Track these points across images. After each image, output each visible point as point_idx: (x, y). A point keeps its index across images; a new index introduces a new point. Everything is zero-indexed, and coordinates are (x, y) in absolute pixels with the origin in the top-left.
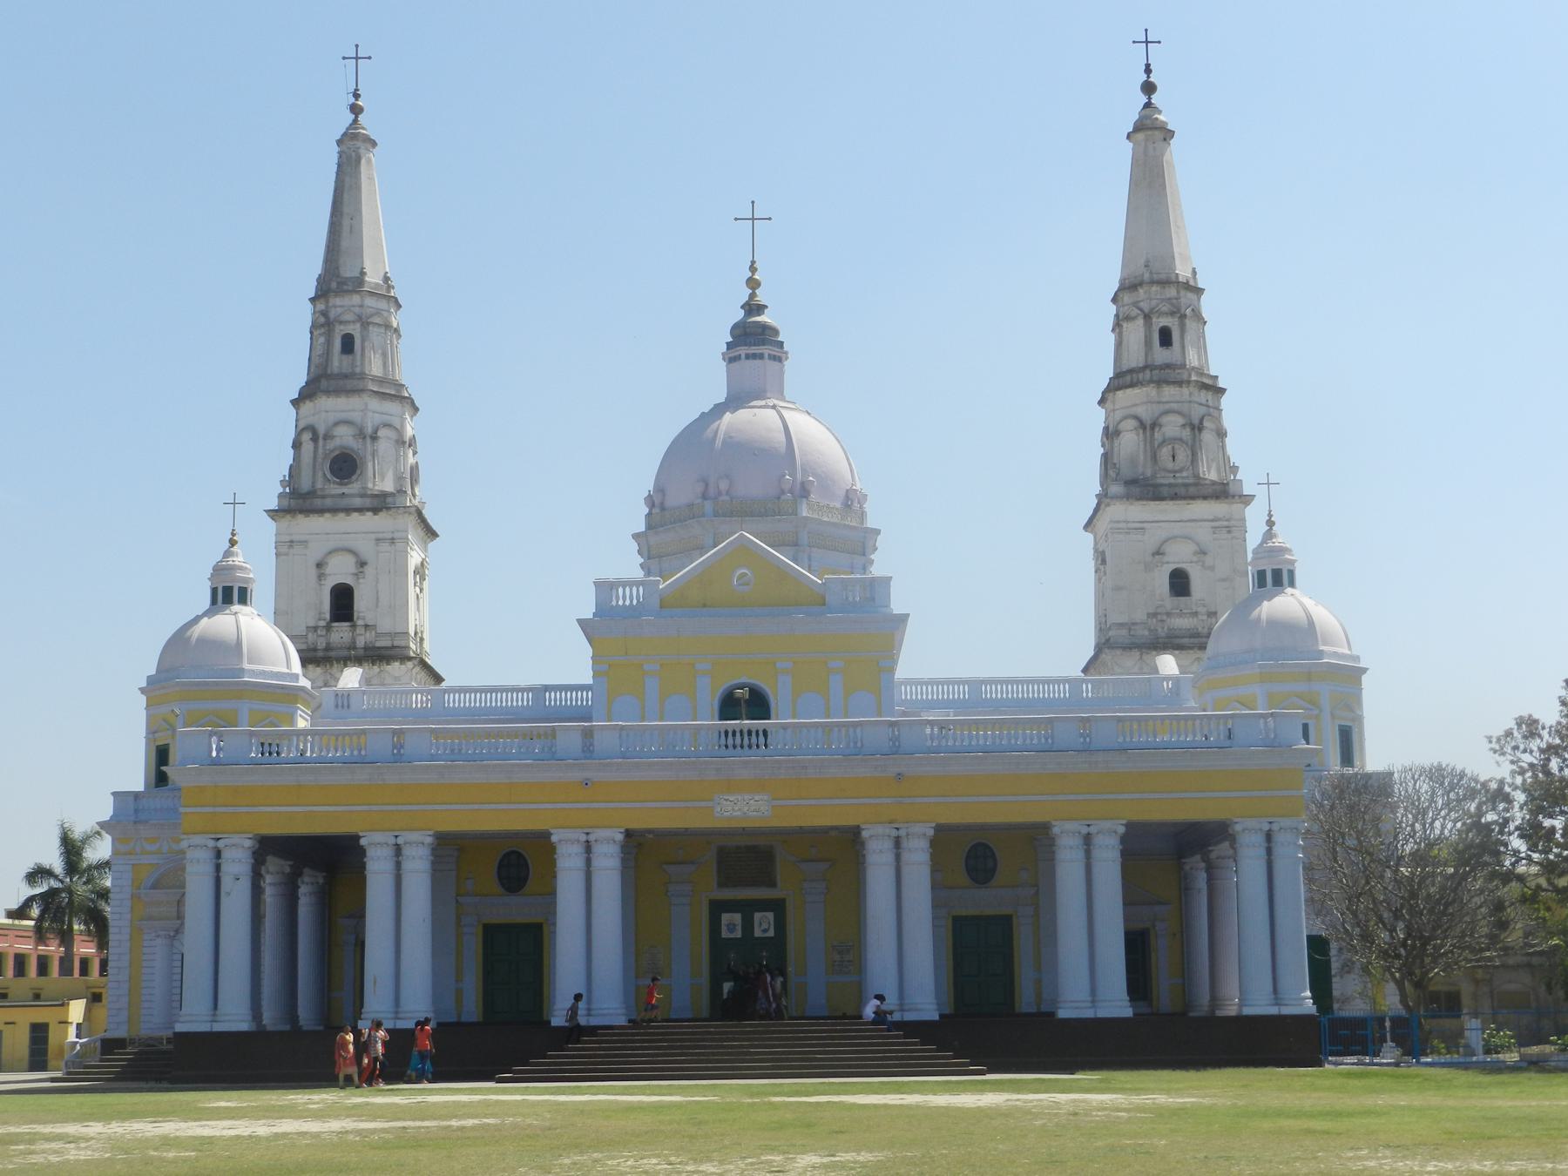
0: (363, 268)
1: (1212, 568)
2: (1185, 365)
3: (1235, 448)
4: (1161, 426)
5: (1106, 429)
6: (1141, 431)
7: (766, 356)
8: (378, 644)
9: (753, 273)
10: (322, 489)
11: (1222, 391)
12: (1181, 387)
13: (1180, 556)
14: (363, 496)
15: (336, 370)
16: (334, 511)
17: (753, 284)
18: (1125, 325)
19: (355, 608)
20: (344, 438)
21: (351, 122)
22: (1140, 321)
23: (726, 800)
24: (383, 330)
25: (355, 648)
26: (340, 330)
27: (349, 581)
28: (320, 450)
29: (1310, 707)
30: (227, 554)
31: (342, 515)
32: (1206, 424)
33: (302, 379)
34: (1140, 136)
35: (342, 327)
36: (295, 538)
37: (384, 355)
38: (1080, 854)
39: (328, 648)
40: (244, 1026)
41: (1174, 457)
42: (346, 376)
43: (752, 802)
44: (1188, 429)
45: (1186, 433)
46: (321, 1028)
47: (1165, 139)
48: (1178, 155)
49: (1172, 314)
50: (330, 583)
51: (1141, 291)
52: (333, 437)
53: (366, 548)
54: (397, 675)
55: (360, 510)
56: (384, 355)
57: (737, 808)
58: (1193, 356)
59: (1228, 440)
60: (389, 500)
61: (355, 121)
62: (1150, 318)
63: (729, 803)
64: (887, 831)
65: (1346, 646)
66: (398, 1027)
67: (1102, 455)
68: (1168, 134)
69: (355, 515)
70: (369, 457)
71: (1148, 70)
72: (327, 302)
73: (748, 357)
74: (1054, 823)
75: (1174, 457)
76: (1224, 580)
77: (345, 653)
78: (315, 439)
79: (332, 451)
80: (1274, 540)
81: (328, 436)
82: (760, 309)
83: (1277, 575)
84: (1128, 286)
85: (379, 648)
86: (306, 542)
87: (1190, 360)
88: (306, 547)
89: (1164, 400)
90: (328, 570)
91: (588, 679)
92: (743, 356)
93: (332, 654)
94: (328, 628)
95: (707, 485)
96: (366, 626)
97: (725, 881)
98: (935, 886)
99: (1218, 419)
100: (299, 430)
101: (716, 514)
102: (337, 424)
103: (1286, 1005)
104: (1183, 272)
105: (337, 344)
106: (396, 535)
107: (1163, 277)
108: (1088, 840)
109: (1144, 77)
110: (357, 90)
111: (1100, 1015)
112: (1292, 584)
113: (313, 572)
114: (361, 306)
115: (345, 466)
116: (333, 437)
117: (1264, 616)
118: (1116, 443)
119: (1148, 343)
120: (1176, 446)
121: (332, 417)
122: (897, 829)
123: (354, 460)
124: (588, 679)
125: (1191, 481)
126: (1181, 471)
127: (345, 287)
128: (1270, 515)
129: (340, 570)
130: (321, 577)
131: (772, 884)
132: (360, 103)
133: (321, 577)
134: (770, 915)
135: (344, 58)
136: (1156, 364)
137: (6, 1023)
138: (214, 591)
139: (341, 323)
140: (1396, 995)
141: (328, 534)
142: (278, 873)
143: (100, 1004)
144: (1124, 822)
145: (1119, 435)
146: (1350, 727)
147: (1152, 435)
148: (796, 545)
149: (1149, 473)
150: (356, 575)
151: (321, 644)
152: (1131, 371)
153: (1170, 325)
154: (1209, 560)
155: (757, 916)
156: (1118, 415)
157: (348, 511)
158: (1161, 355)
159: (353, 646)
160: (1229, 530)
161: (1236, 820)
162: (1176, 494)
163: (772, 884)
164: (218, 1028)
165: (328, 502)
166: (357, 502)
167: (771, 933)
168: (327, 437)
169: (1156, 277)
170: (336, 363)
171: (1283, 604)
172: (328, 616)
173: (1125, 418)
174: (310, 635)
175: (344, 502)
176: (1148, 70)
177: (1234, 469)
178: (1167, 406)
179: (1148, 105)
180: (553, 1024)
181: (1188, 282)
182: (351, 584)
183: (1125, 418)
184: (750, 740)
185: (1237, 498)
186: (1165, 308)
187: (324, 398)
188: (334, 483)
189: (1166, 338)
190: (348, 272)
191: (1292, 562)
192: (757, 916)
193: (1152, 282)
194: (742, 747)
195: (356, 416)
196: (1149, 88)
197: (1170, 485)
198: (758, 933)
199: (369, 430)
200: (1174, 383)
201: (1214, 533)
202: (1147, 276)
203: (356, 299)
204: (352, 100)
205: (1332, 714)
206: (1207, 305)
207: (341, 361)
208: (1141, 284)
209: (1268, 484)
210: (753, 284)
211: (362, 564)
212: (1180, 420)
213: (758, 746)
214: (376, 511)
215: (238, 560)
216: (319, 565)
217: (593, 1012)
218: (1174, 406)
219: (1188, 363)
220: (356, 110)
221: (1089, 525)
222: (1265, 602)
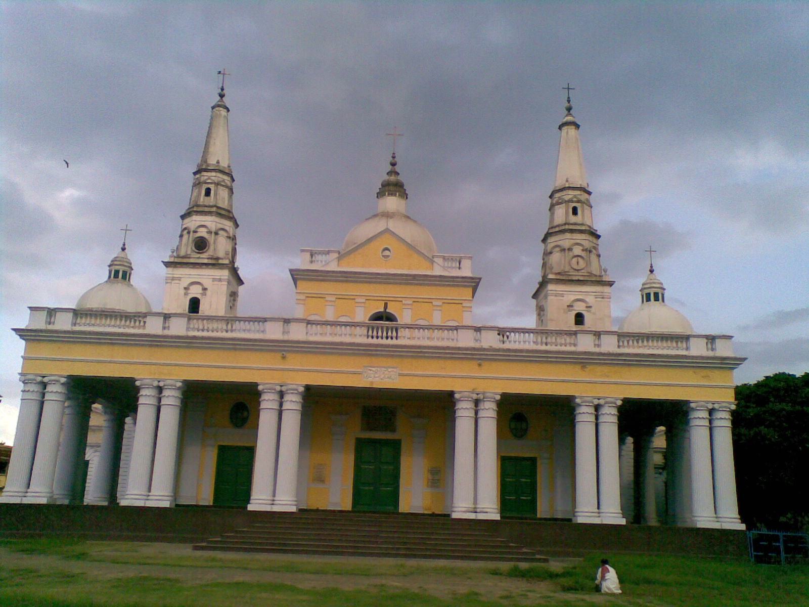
1: (594, 314)
10: (190, 254)
13: (580, 308)
15: (201, 204)
23: (370, 370)
40: (166, 504)
41: (578, 263)
43: (386, 372)
46: (106, 504)
50: (190, 296)
63: (372, 372)
78: (189, 233)
100: (183, 228)
111: (605, 522)
129: (195, 292)
130: (186, 294)
131: (394, 430)
140: (498, 513)
152: (558, 226)
153: (577, 206)
154: (593, 310)
158: (573, 219)
165: (192, 261)
168: (195, 232)
170: (202, 200)
184: (387, 334)
194: (382, 338)
204: (220, 91)
209: (651, 251)
211: (205, 289)
221: (535, 296)
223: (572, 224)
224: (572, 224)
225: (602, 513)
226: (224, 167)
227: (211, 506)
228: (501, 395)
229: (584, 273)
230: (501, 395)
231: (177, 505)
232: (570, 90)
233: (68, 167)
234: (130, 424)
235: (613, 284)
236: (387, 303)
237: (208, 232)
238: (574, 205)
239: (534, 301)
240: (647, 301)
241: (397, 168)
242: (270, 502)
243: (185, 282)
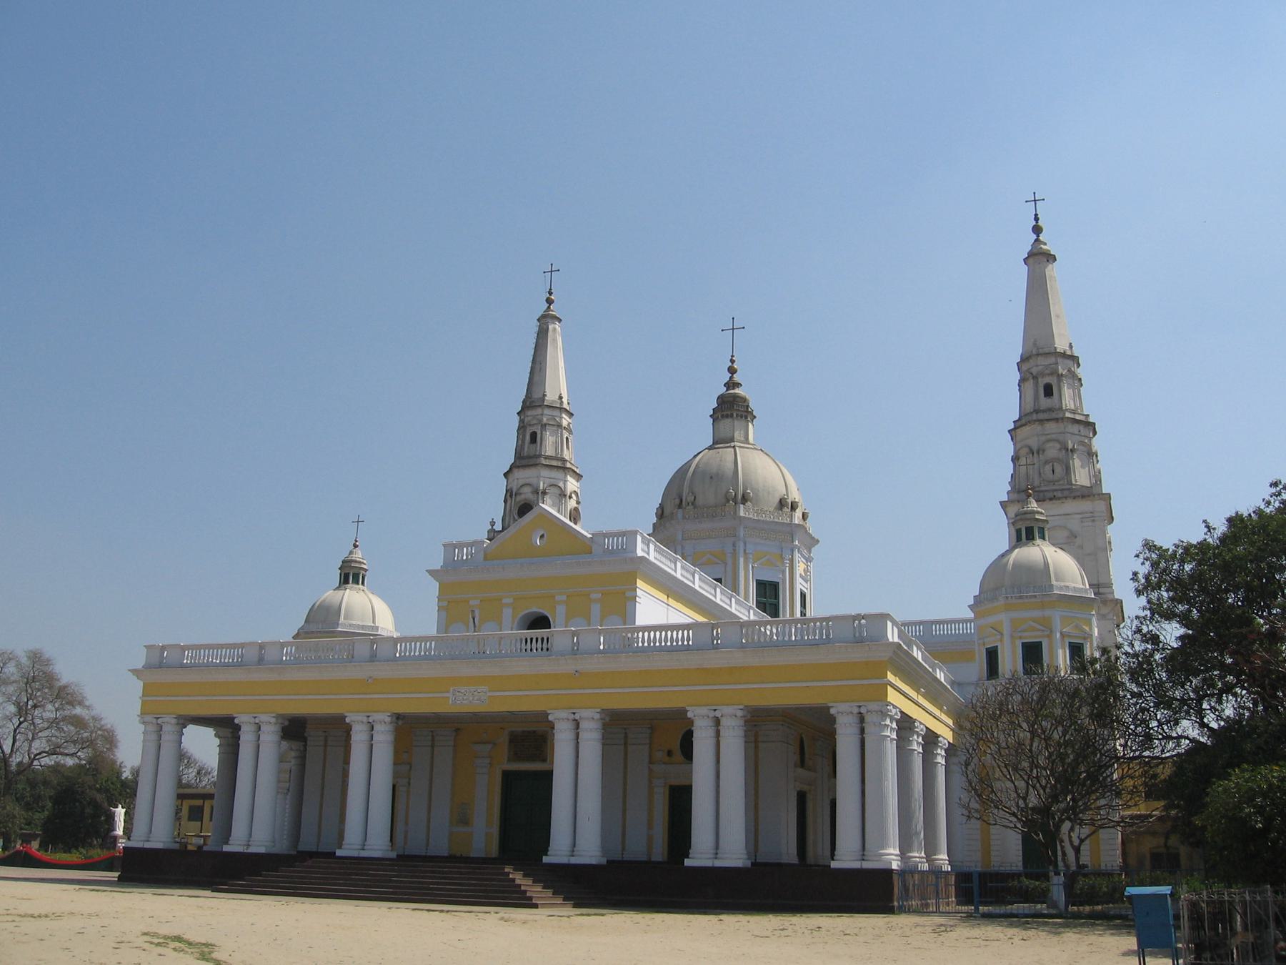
2: (1062, 408)
4: (1044, 451)
9: (732, 363)
17: (732, 371)
20: (527, 494)
24: (555, 428)
29: (1043, 629)
30: (351, 553)
33: (511, 459)
34: (1031, 260)
38: (711, 732)
41: (1053, 471)
43: (476, 693)
47: (1048, 261)
48: (1054, 272)
49: (1051, 374)
52: (520, 494)
57: (465, 698)
58: (1069, 402)
62: (1037, 378)
68: (1051, 258)
71: (1036, 219)
75: (1053, 471)
76: (1089, 554)
79: (520, 502)
80: (1029, 506)
82: (738, 385)
84: (1024, 359)
87: (1066, 404)
89: (1046, 433)
91: (433, 632)
97: (516, 756)
102: (522, 486)
103: (867, 860)
104: (1061, 345)
105: (528, 438)
107: (1046, 350)
109: (1034, 223)
110: (551, 289)
116: (520, 494)
119: (1036, 398)
121: (521, 482)
122: (574, 713)
123: (525, 503)
124: (433, 632)
132: (552, 297)
136: (1041, 409)
139: (530, 425)
142: (297, 750)
145: (1018, 459)
153: (1051, 382)
158: (1045, 402)
161: (830, 705)
162: (1054, 496)
164: (718, 863)
169: (1041, 351)
176: (1036, 219)
178: (1049, 437)
179: (1037, 240)
180: (832, 866)
181: (1065, 352)
185: (1096, 496)
189: (1048, 391)
195: (533, 481)
196: (1037, 230)
201: (1082, 522)
207: (528, 448)
210: (732, 371)
213: (531, 650)
215: (358, 555)
217: (365, 847)
219: (1064, 406)
223: (1044, 411)
224: (1044, 411)
225: (709, 858)
226: (553, 401)
227: (494, 859)
228: (290, 721)
229: (1063, 485)
230: (290, 721)
231: (298, 852)
234: (751, 742)
237: (532, 493)
238: (1047, 380)
241: (737, 378)
242: (360, 847)
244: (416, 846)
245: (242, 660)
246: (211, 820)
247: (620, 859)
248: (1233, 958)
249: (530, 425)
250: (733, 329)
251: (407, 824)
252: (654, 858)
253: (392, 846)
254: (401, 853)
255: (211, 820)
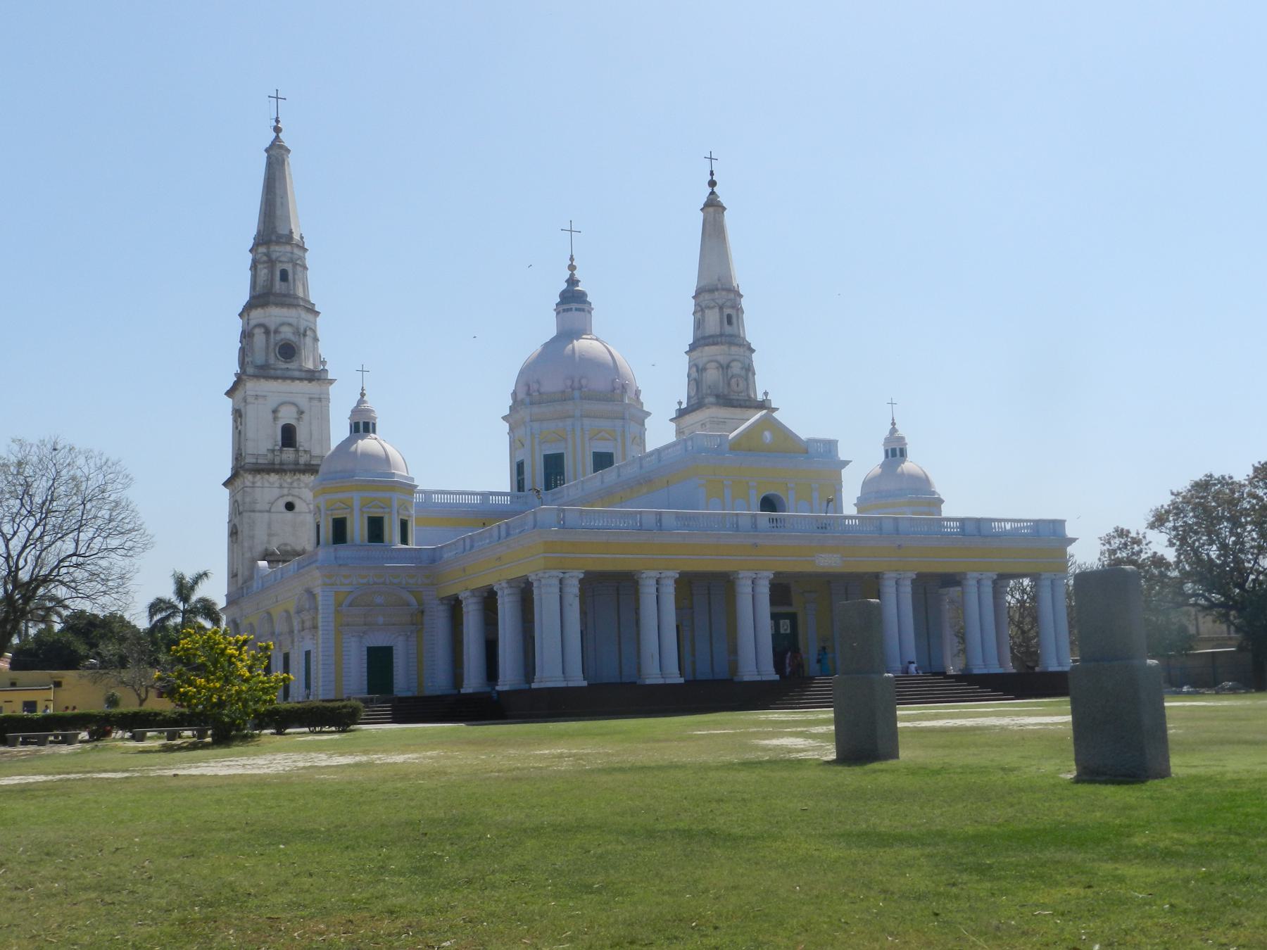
0: (291, 230)
3: (324, 349)
5: (243, 333)
6: (721, 370)
7: (574, 309)
8: (313, 462)
11: (318, 313)
12: (740, 347)
14: (301, 370)
15: (278, 292)
16: (284, 378)
17: (572, 268)
18: (706, 311)
19: (297, 439)
20: (287, 333)
21: (274, 137)
22: (717, 310)
25: (298, 464)
26: (279, 267)
27: (293, 422)
28: (272, 340)
31: (289, 382)
32: (308, 333)
34: (711, 210)
35: (281, 265)
36: (259, 393)
37: (303, 285)
39: (281, 464)
42: (285, 296)
44: (744, 370)
45: (743, 373)
50: (281, 423)
51: (716, 293)
53: (303, 403)
54: (307, 482)
55: (301, 379)
56: (303, 285)
59: (756, 376)
60: (317, 374)
61: (277, 137)
64: (673, 575)
65: (406, 470)
66: (569, 685)
67: (240, 348)
69: (297, 382)
70: (302, 347)
71: (712, 173)
72: (268, 248)
73: (576, 310)
74: (740, 572)
77: (291, 467)
81: (276, 332)
83: (366, 425)
85: (313, 465)
86: (266, 396)
88: (266, 400)
90: (280, 415)
91: (508, 490)
92: (574, 309)
93: (285, 467)
94: (281, 451)
95: (573, 381)
96: (305, 451)
98: (676, 609)
99: (314, 331)
101: (581, 398)
102: (283, 324)
106: (322, 396)
108: (979, 582)
112: (374, 432)
113: (270, 416)
114: (292, 253)
115: (288, 351)
116: (280, 332)
117: (359, 451)
118: (704, 375)
120: (739, 379)
124: (508, 490)
125: (746, 398)
126: (741, 392)
127: (281, 240)
128: (893, 420)
129: (287, 416)
130: (275, 419)
131: (791, 605)
133: (275, 419)
134: (788, 622)
135: (269, 97)
137: (6, 702)
138: (887, 452)
139: (280, 262)
141: (279, 392)
143: (60, 688)
144: (583, 571)
146: (407, 520)
147: (727, 372)
148: (624, 419)
149: (726, 392)
150: (298, 419)
151: (277, 460)
155: (782, 622)
156: (253, 323)
157: (293, 379)
159: (297, 463)
160: (320, 400)
163: (791, 605)
165: (279, 373)
166: (297, 374)
167: (788, 631)
168: (276, 332)
171: (367, 444)
172: (280, 443)
173: (712, 361)
174: (269, 455)
175: (289, 373)
176: (712, 173)
177: (324, 363)
179: (712, 193)
182: (294, 424)
183: (712, 361)
186: (729, 304)
187: (274, 307)
188: (282, 361)
189: (730, 322)
190: (282, 231)
191: (375, 418)
192: (782, 622)
193: (723, 289)
196: (712, 183)
197: (738, 400)
198: (782, 631)
199: (302, 330)
200: (737, 345)
202: (719, 286)
203: (288, 248)
204: (275, 124)
205: (398, 512)
206: (309, 259)
208: (717, 290)
212: (739, 365)
214: (310, 380)
216: (275, 411)
218: (737, 357)
220: (277, 130)
221: (230, 393)
222: (360, 441)
232: (569, 229)
233: (205, 574)
235: (331, 384)
236: (519, 490)
239: (229, 401)
240: (355, 432)
243: (271, 404)
244: (703, 672)
245: (564, 523)
246: (308, 654)
247: (619, 681)
248: (48, 788)
249: (280, 262)
250: (571, 231)
251: (694, 655)
252: (700, 677)
253: (680, 674)
254: (691, 678)
255: (308, 654)
